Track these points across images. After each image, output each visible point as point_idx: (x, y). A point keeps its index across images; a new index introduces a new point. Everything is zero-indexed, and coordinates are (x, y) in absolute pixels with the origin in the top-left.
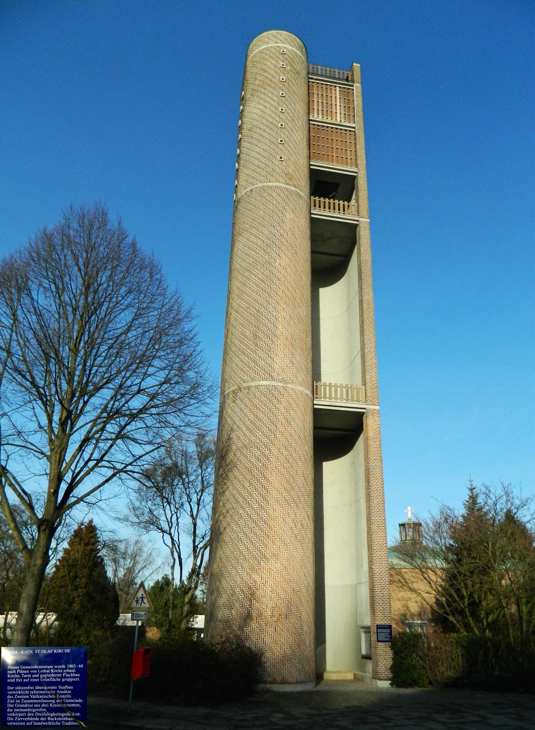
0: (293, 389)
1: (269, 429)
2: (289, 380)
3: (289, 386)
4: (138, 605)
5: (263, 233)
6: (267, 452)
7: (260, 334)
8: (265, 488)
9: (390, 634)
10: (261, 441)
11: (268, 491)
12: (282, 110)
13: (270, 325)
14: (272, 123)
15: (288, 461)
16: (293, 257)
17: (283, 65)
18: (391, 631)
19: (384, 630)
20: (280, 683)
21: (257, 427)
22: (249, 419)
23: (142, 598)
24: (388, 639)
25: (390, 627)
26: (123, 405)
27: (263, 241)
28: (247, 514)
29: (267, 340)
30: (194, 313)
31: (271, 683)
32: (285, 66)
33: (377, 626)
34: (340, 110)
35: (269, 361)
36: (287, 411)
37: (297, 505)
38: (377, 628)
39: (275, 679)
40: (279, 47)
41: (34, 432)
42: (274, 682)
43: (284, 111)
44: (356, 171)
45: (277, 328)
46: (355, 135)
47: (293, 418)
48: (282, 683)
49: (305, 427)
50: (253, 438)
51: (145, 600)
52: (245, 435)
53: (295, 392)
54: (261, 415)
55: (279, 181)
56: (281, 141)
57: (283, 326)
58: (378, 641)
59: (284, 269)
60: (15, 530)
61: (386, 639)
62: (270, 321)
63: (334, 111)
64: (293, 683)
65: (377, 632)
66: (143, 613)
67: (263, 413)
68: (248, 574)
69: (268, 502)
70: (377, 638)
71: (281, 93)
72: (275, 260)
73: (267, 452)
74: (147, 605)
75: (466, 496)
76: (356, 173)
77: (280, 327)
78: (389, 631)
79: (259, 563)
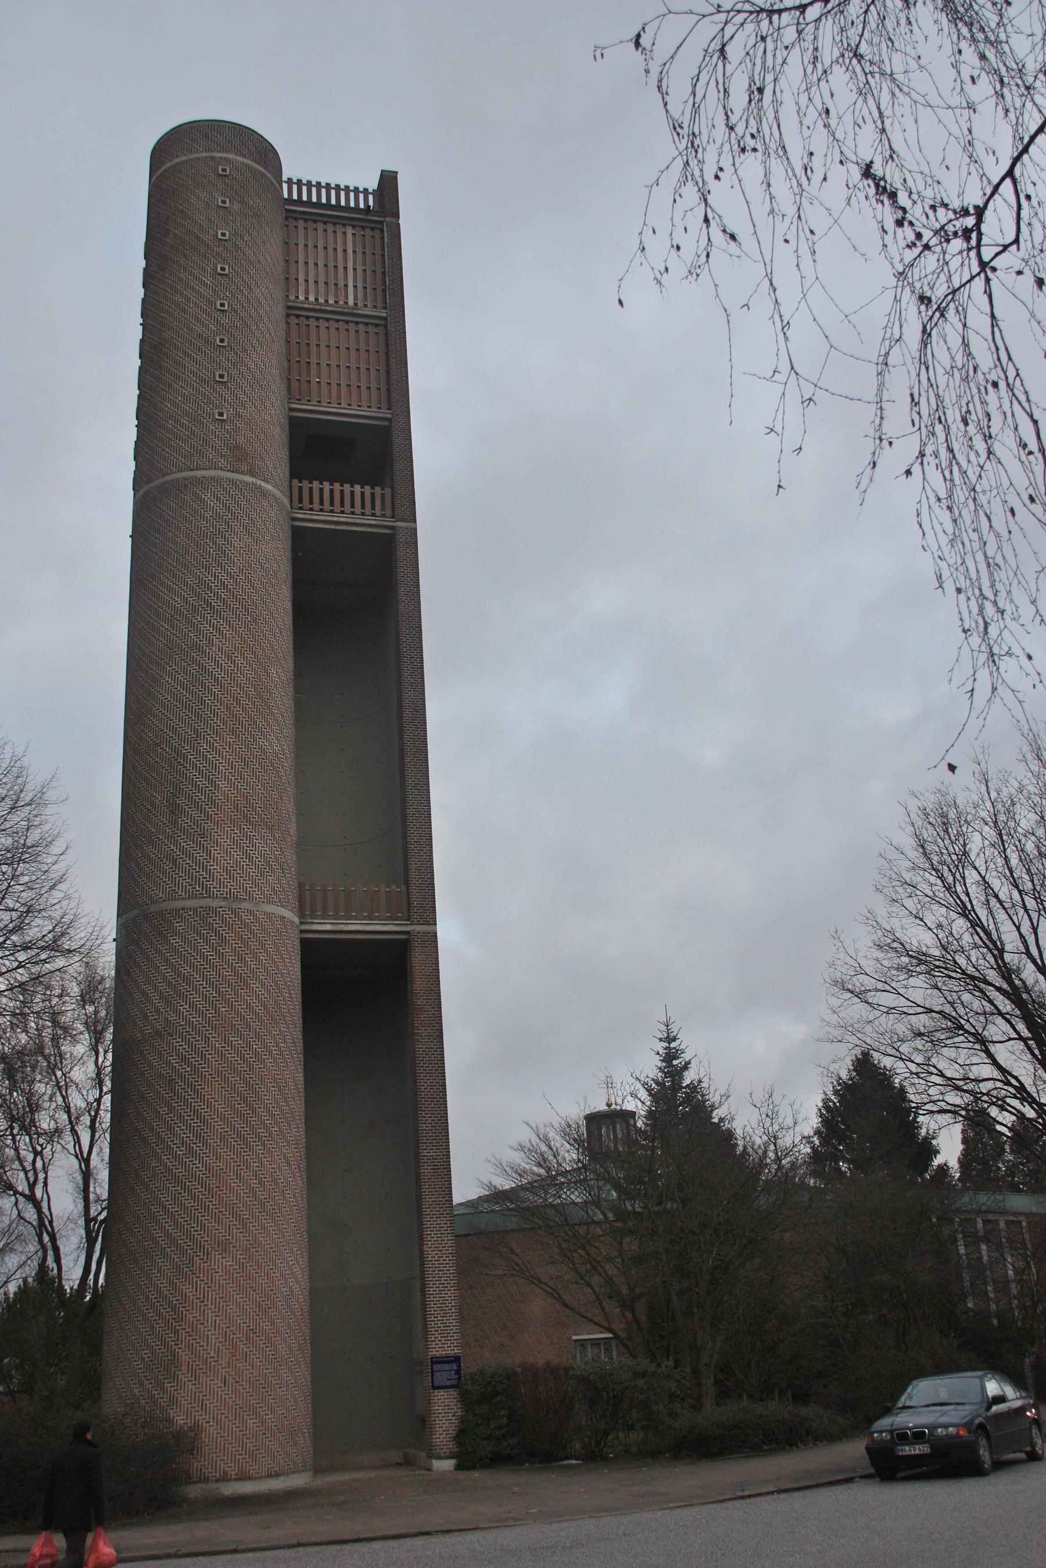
0: (250, 912)
1: (205, 998)
2: (242, 895)
3: (244, 905)
5: (186, 584)
7: (182, 801)
8: (199, 1115)
9: (458, 1372)
10: (189, 1023)
11: (205, 1122)
12: (222, 305)
13: (201, 782)
14: (200, 336)
16: (249, 630)
17: (224, 202)
18: (459, 1366)
19: (446, 1367)
20: (235, 1480)
21: (180, 995)
22: (165, 978)
24: (454, 1382)
27: (185, 600)
28: (165, 1166)
29: (196, 814)
30: (51, 795)
31: (217, 1481)
32: (227, 205)
33: (432, 1359)
34: (354, 245)
35: (201, 856)
36: (241, 959)
37: (264, 1145)
38: (433, 1363)
39: (225, 1473)
40: (213, 158)
42: (225, 1478)
43: (226, 308)
44: (389, 416)
45: (217, 787)
46: (386, 334)
47: (252, 971)
48: (240, 1479)
49: (277, 986)
50: (173, 1017)
52: (157, 1011)
54: (186, 970)
56: (221, 376)
57: (230, 782)
58: (434, 1388)
61: (449, 1383)
62: (201, 772)
63: (341, 284)
64: (261, 1478)
65: (432, 1372)
67: (192, 966)
68: (171, 1283)
69: (205, 1143)
70: (433, 1382)
71: (217, 374)
72: (210, 642)
73: (201, 1045)
75: (651, 1067)
76: (389, 420)
77: (222, 784)
78: (455, 1367)
79: (191, 1261)
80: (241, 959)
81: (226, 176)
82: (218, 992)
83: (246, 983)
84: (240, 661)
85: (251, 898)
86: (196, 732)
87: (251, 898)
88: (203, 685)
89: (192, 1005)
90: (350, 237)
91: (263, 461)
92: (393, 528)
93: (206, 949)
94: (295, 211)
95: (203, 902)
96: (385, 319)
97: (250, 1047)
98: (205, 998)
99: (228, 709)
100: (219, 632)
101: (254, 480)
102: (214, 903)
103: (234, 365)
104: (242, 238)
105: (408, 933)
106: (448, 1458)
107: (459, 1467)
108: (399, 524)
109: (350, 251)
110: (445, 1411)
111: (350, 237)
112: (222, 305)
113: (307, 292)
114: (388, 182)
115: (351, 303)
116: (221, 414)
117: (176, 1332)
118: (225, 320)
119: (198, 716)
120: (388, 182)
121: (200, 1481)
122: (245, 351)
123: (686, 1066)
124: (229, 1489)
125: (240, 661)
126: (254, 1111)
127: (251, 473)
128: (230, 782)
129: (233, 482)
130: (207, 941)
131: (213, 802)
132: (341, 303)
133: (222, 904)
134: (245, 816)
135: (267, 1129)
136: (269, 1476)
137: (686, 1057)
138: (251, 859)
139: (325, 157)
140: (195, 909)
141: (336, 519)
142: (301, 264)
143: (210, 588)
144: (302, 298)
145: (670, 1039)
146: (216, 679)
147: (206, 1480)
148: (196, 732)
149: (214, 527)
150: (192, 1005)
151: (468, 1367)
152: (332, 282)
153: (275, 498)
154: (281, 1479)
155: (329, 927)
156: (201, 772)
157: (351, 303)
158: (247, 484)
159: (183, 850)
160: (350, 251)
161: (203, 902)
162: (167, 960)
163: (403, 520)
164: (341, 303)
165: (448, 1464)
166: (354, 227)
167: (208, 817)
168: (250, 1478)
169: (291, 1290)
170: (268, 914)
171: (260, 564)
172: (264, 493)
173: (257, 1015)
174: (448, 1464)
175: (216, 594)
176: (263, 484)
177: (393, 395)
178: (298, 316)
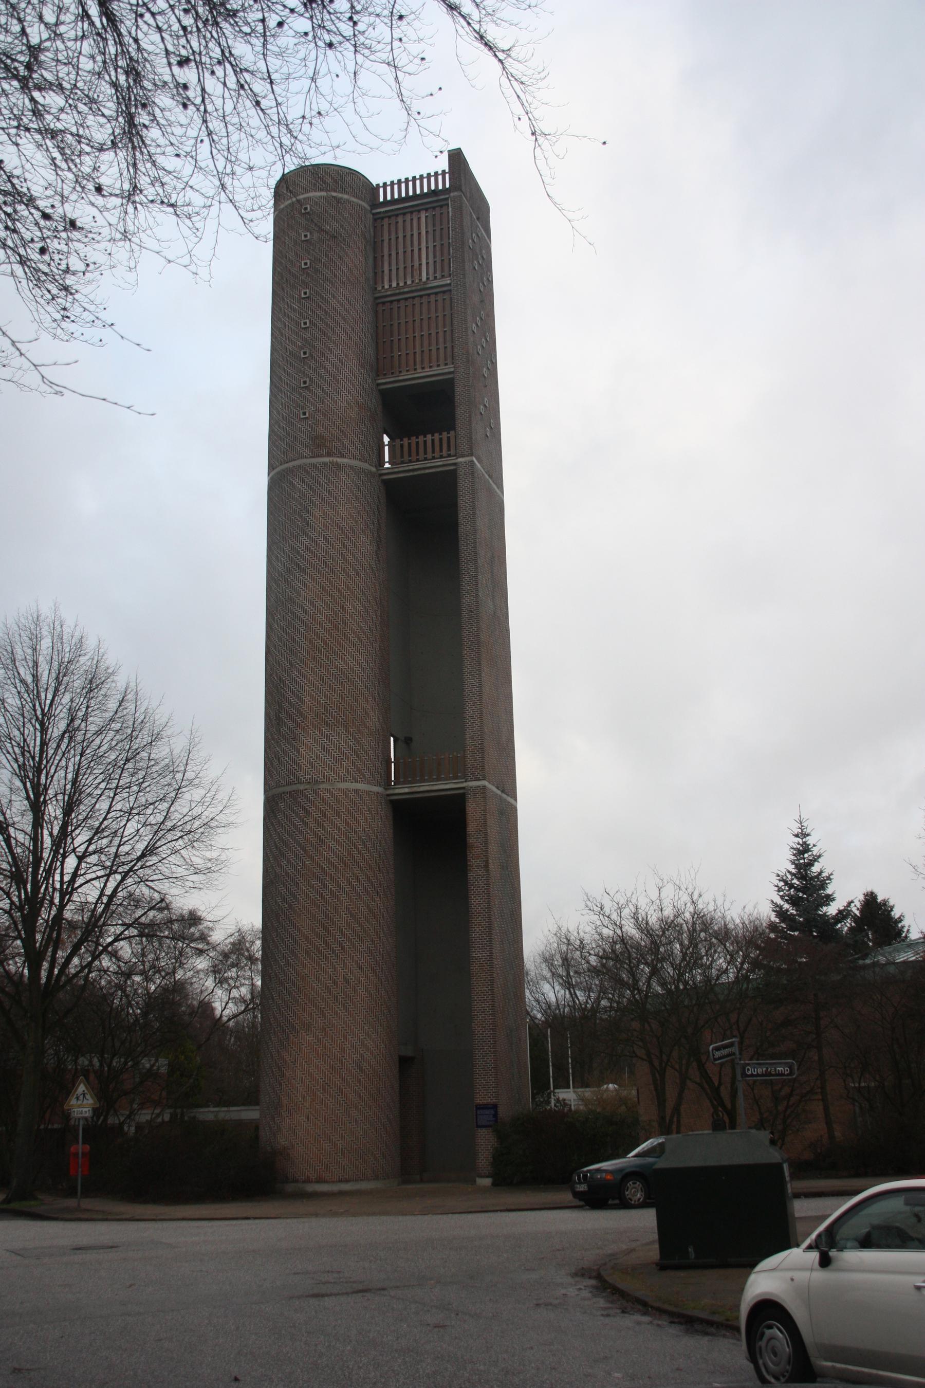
1: (296, 856)
3: (321, 786)
4: (79, 1102)
6: (294, 888)
7: (283, 715)
9: (495, 1115)
13: (293, 700)
15: (321, 895)
16: (327, 579)
17: (306, 236)
18: (496, 1112)
19: (487, 1112)
23: (84, 1095)
25: (495, 1107)
26: (62, 907)
29: (290, 724)
31: (304, 1182)
36: (320, 825)
41: (538, 150)
42: (308, 1181)
44: (452, 370)
51: (88, 1096)
53: (333, 795)
54: (285, 836)
55: (303, 457)
57: (312, 696)
58: (478, 1126)
59: (312, 603)
60: (151, 920)
62: (293, 692)
64: (333, 1182)
66: (87, 1109)
68: (278, 1052)
73: (294, 888)
74: (91, 1101)
75: (785, 864)
78: (492, 1112)
80: (320, 825)
81: (308, 213)
82: (304, 850)
83: (324, 843)
84: (319, 604)
85: (328, 780)
86: (291, 664)
87: (328, 780)
88: (294, 627)
89: (289, 861)
90: (423, 220)
91: (339, 440)
92: (455, 464)
93: (297, 821)
94: (380, 213)
95: (294, 787)
96: (450, 284)
97: (326, 886)
98: (296, 856)
99: (311, 642)
100: (305, 585)
101: (331, 459)
102: (301, 787)
103: (315, 370)
104: (320, 261)
105: (464, 788)
106: (487, 1177)
107: (494, 1184)
108: (460, 460)
109: (423, 233)
110: (485, 1143)
111: (423, 220)
112: (305, 323)
113: (390, 281)
114: (457, 159)
115: (424, 279)
116: (304, 414)
117: (281, 1084)
118: (308, 335)
119: (291, 651)
120: (457, 159)
121: (293, 1182)
122: (323, 355)
123: (816, 858)
124: (310, 1188)
125: (319, 604)
126: (329, 932)
127: (329, 454)
128: (312, 696)
129: (314, 466)
130: (297, 815)
131: (301, 714)
132: (417, 281)
133: (307, 787)
134: (323, 721)
135: (340, 944)
136: (340, 1181)
137: (815, 851)
138: (327, 751)
139: (395, 161)
140: (290, 792)
141: (411, 468)
142: (386, 258)
143: (298, 553)
144: (386, 287)
145: (803, 834)
146: (303, 622)
147: (297, 1181)
148: (291, 664)
149: (301, 504)
150: (289, 861)
151: (504, 1112)
152: (409, 265)
153: (351, 467)
154: (350, 1184)
155: (406, 790)
156: (293, 692)
157: (424, 279)
158: (325, 464)
159: (283, 751)
160: (423, 233)
161: (294, 787)
162: (276, 830)
163: (463, 456)
164: (417, 281)
165: (487, 1182)
166: (426, 210)
167: (298, 725)
168: (326, 1182)
169: (362, 1056)
170: (342, 790)
171: (337, 525)
172: (339, 467)
173: (333, 864)
174: (487, 1182)
175: (302, 556)
176: (339, 460)
177: (456, 350)
178: (384, 303)
